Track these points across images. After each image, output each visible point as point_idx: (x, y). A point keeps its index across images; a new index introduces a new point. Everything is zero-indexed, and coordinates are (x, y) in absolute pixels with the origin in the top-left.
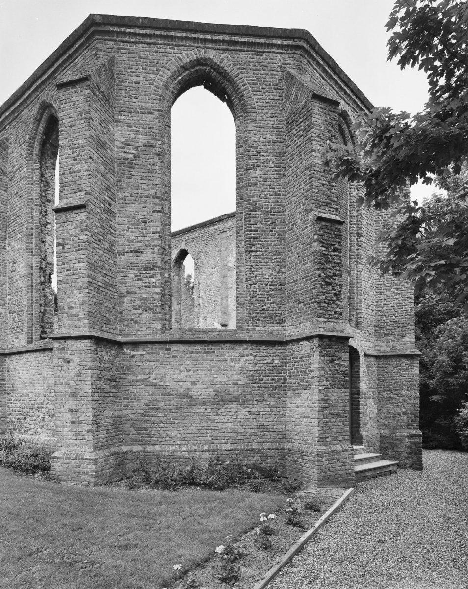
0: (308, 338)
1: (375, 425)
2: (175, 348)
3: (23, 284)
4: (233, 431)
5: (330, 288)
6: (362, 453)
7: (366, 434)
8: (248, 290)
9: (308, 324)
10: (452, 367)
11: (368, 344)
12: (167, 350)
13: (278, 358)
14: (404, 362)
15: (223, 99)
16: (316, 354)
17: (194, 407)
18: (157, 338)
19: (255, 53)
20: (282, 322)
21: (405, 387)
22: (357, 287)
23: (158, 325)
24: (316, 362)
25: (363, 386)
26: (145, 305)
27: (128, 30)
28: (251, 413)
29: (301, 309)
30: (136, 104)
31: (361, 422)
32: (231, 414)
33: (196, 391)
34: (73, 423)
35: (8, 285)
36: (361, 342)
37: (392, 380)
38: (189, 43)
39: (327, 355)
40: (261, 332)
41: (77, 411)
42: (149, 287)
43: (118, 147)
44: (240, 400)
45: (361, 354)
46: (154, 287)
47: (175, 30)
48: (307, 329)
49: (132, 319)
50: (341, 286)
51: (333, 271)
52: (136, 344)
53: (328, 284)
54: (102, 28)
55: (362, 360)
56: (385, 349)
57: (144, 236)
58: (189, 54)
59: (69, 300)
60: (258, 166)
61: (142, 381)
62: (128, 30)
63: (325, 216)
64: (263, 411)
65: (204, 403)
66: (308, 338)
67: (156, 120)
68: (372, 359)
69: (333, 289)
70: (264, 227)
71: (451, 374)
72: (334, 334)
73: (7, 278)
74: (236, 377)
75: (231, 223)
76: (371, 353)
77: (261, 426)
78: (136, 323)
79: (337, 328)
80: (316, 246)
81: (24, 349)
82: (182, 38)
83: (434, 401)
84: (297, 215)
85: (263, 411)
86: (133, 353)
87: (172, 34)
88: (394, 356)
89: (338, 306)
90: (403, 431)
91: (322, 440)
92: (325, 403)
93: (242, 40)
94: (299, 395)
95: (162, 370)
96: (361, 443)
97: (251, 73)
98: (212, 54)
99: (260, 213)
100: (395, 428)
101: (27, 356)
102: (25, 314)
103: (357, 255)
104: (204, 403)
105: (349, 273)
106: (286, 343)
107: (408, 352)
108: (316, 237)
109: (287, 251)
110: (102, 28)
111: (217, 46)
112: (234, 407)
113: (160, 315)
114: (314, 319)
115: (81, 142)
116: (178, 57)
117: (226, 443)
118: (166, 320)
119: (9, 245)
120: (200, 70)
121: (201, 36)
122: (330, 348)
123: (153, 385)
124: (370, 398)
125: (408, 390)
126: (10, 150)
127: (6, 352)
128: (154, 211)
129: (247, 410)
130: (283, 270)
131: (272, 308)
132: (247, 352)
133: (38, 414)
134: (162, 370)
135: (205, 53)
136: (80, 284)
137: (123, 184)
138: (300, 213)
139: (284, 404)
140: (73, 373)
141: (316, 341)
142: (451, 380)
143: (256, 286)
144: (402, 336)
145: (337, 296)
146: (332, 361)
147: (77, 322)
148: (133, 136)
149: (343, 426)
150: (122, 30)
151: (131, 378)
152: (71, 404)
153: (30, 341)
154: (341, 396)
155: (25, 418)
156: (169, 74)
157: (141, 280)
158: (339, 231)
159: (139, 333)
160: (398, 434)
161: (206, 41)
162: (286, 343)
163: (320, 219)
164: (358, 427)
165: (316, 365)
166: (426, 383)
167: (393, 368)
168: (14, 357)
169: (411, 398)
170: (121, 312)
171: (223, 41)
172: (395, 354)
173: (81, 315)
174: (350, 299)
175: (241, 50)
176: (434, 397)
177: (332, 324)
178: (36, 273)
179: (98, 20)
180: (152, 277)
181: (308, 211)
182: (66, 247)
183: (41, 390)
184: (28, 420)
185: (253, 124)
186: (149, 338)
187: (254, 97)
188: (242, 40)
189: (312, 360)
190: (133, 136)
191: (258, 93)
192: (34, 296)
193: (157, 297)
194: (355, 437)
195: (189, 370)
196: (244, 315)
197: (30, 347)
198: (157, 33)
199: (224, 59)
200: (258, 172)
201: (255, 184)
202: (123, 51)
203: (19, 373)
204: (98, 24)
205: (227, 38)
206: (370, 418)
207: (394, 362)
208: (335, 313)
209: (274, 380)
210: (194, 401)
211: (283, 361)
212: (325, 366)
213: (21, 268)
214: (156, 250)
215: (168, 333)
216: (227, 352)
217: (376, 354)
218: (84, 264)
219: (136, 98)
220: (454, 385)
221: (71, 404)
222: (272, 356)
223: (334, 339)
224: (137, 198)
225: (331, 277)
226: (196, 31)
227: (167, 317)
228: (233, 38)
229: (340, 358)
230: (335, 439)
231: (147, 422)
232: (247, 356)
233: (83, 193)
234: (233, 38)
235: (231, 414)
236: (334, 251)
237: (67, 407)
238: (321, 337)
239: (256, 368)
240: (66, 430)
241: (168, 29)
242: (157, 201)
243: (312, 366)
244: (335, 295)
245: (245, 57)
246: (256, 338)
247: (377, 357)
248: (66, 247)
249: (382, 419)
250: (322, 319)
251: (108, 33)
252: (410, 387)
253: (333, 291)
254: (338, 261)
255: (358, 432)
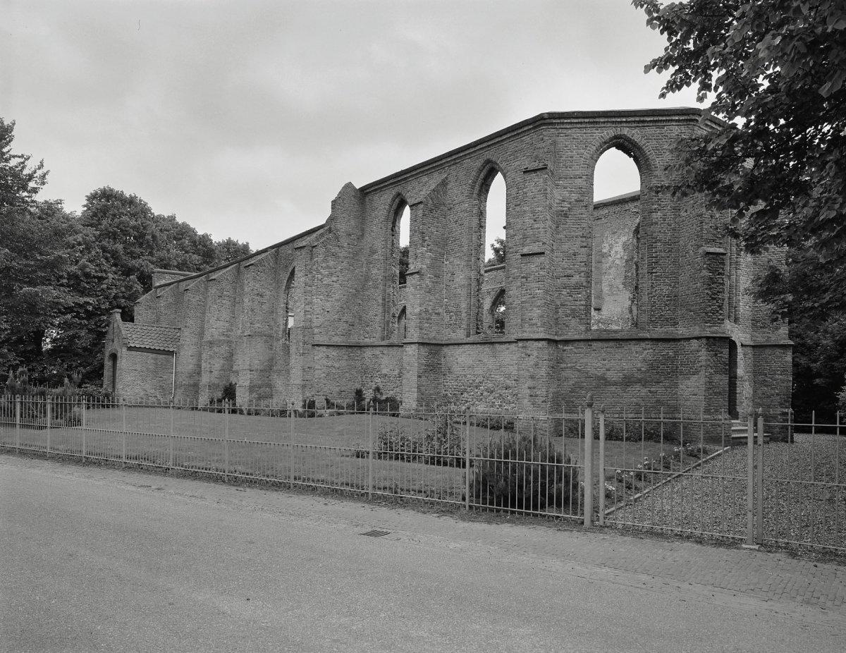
0: (698, 338)
1: (751, 404)
2: (595, 344)
3: (463, 292)
4: (637, 404)
6: (737, 425)
7: (742, 411)
8: (650, 301)
9: (697, 327)
10: (838, 351)
11: (745, 335)
12: (589, 345)
13: (672, 351)
14: (778, 351)
15: (630, 156)
16: (703, 350)
17: (609, 387)
18: (582, 337)
19: (658, 127)
20: (675, 324)
21: (779, 372)
22: (736, 289)
23: (583, 328)
24: (704, 355)
25: (740, 371)
26: (574, 314)
27: (566, 121)
28: (650, 392)
29: (691, 315)
30: (570, 172)
31: (737, 401)
32: (635, 392)
33: (609, 375)
34: (531, 396)
35: (445, 291)
36: (740, 335)
37: (767, 366)
38: (609, 125)
39: (712, 351)
40: (659, 332)
41: (534, 388)
42: (577, 301)
43: (557, 204)
44: (643, 382)
45: (738, 344)
46: (580, 300)
47: (599, 117)
48: (696, 331)
49: (564, 324)
50: (723, 300)
51: (718, 289)
52: (566, 342)
54: (548, 121)
55: (739, 350)
56: (761, 340)
57: (574, 265)
58: (609, 132)
59: (530, 314)
60: (659, 210)
61: (571, 367)
62: (566, 121)
63: (712, 250)
64: (660, 390)
65: (615, 384)
66: (698, 338)
67: (585, 182)
68: (749, 348)
69: (717, 302)
70: (663, 254)
71: (837, 358)
72: (718, 335)
73: (444, 285)
74: (639, 365)
75: (607, 211)
76: (747, 343)
77: (658, 401)
78: (567, 326)
79: (720, 330)
80: (705, 273)
82: (604, 122)
83: (817, 384)
84: (689, 247)
85: (660, 390)
86: (565, 348)
87: (597, 120)
88: (770, 346)
89: (721, 314)
90: (776, 409)
91: (707, 411)
92: (710, 385)
93: (648, 119)
94: (689, 379)
95: (585, 360)
96: (737, 419)
97: (655, 142)
98: (626, 131)
99: (659, 244)
100: (769, 407)
101: (467, 346)
102: (464, 315)
103: (737, 262)
104: (615, 384)
105: (729, 277)
107: (782, 342)
108: (705, 266)
109: (680, 271)
110: (548, 121)
111: (630, 125)
112: (638, 387)
113: (584, 321)
114: (703, 324)
115: (539, 209)
116: (602, 137)
117: (631, 413)
118: (588, 324)
119: (447, 260)
120: (617, 142)
121: (619, 120)
122: (715, 345)
123: (579, 371)
124: (746, 381)
126: (449, 187)
127: (443, 342)
128: (582, 247)
129: (648, 389)
130: (677, 286)
131: (668, 314)
132: (649, 346)
133: (476, 391)
134: (585, 360)
135: (621, 131)
136: (539, 304)
137: (560, 229)
138: (692, 246)
139: (676, 385)
140: (532, 363)
141: (704, 341)
142: (836, 364)
143: (656, 298)
144: (777, 329)
145: (721, 307)
146: (716, 355)
147: (535, 329)
148: (568, 195)
149: (723, 401)
150: (562, 121)
151: (563, 365)
152: (530, 383)
153: (468, 336)
154: (723, 380)
155: (462, 394)
156: (595, 148)
157: (572, 296)
158: (723, 260)
159: (569, 334)
160: (771, 412)
161: (621, 122)
162: (679, 340)
163: (708, 253)
164: (735, 405)
166: (809, 367)
167: (767, 356)
168: (451, 347)
169: (784, 381)
170: (557, 319)
171: (634, 122)
172: (769, 343)
173: (539, 324)
174: (729, 298)
175: (647, 126)
176: (818, 381)
177: (716, 328)
178: (474, 284)
179: (546, 116)
181: (699, 246)
182: (529, 279)
183: (481, 372)
184: (465, 395)
185: (656, 179)
186: (577, 337)
187: (657, 159)
188: (648, 119)
189: (700, 354)
190: (568, 195)
191: (660, 156)
192: (472, 301)
193: (582, 307)
194: (733, 413)
195: (604, 360)
197: (471, 339)
198: (587, 120)
199: (635, 134)
200: (659, 214)
201: (656, 223)
202: (561, 135)
203: (457, 359)
204: (545, 119)
205: (637, 119)
206: (746, 398)
207: (768, 351)
208: (718, 319)
209: (669, 367)
210: (609, 382)
211: (676, 353)
212: (709, 358)
213: (460, 278)
214: (582, 274)
215: (589, 333)
216: (634, 347)
217: (752, 344)
218: (542, 291)
219: (570, 168)
220: (839, 369)
221: (530, 383)
222: (668, 350)
223: (717, 339)
224: (569, 238)
225: (714, 294)
226: (615, 117)
227: (589, 321)
228: (642, 119)
229: (722, 353)
230: (716, 411)
231: (573, 397)
232: (649, 349)
233: (541, 243)
234: (642, 119)
235: (635, 392)
236: (718, 275)
237: (526, 385)
238: (708, 338)
239: (655, 358)
240: (526, 401)
241: (595, 117)
242: (584, 239)
243: (701, 358)
244: (719, 306)
245: (650, 131)
246: (655, 336)
247: (753, 346)
248: (529, 279)
249: (756, 400)
250: (709, 324)
251: (552, 124)
252: (784, 372)
253: (717, 304)
254: (722, 282)
255: (735, 409)
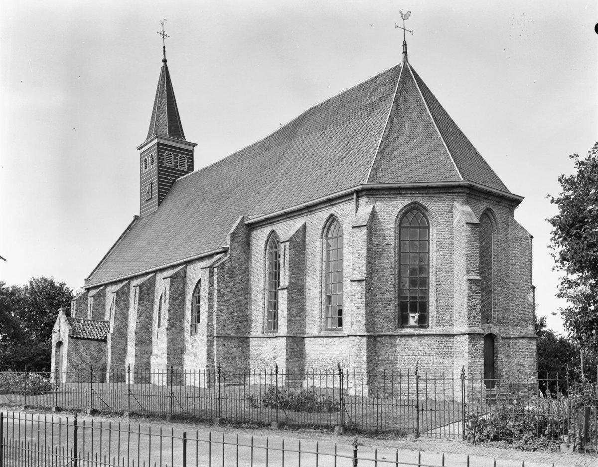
5: (474, 311)
53: (474, 309)
81: (316, 335)
101: (337, 338)
106: (453, 335)
125: (529, 358)
141: (285, 339)
153: (320, 331)
165: (467, 347)
180: (390, 305)
196: (139, 315)
197: (321, 335)
242: (392, 270)
